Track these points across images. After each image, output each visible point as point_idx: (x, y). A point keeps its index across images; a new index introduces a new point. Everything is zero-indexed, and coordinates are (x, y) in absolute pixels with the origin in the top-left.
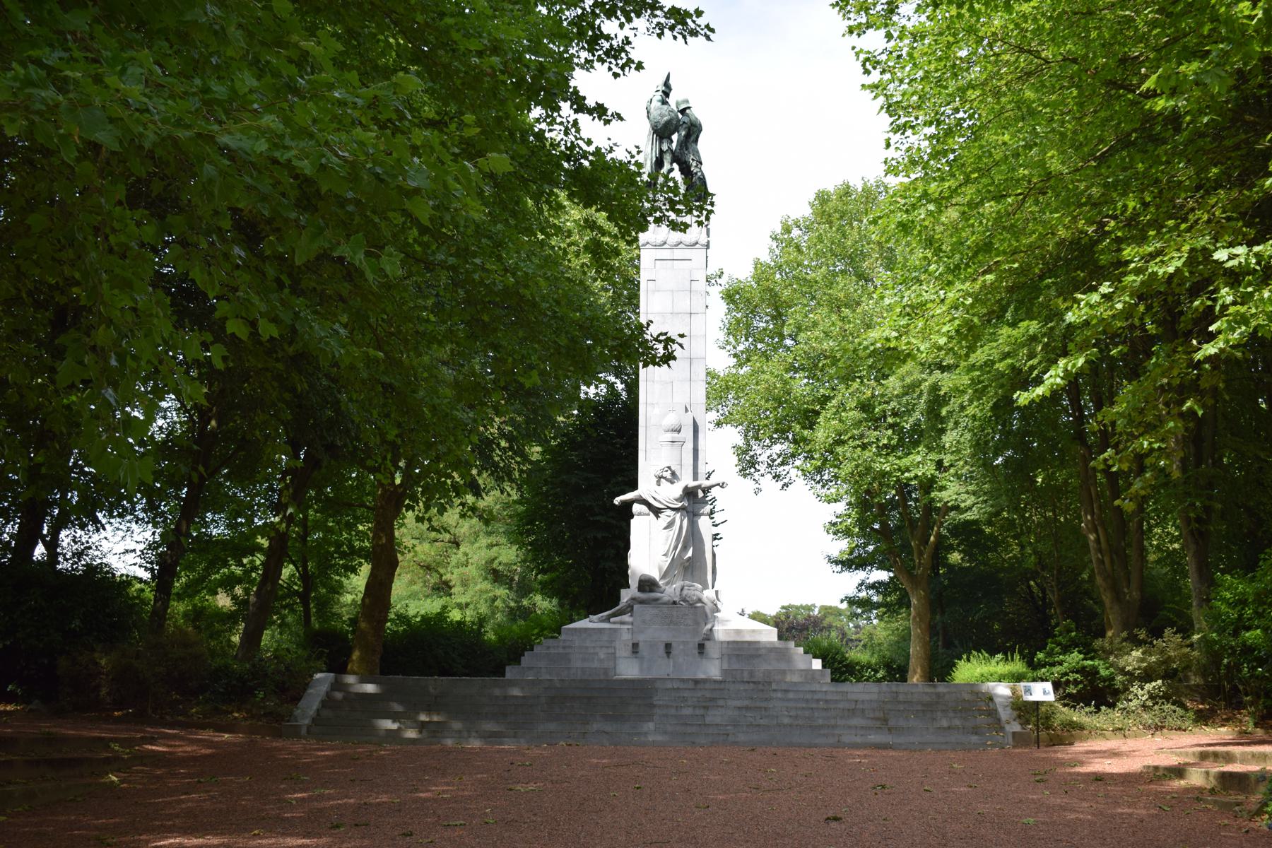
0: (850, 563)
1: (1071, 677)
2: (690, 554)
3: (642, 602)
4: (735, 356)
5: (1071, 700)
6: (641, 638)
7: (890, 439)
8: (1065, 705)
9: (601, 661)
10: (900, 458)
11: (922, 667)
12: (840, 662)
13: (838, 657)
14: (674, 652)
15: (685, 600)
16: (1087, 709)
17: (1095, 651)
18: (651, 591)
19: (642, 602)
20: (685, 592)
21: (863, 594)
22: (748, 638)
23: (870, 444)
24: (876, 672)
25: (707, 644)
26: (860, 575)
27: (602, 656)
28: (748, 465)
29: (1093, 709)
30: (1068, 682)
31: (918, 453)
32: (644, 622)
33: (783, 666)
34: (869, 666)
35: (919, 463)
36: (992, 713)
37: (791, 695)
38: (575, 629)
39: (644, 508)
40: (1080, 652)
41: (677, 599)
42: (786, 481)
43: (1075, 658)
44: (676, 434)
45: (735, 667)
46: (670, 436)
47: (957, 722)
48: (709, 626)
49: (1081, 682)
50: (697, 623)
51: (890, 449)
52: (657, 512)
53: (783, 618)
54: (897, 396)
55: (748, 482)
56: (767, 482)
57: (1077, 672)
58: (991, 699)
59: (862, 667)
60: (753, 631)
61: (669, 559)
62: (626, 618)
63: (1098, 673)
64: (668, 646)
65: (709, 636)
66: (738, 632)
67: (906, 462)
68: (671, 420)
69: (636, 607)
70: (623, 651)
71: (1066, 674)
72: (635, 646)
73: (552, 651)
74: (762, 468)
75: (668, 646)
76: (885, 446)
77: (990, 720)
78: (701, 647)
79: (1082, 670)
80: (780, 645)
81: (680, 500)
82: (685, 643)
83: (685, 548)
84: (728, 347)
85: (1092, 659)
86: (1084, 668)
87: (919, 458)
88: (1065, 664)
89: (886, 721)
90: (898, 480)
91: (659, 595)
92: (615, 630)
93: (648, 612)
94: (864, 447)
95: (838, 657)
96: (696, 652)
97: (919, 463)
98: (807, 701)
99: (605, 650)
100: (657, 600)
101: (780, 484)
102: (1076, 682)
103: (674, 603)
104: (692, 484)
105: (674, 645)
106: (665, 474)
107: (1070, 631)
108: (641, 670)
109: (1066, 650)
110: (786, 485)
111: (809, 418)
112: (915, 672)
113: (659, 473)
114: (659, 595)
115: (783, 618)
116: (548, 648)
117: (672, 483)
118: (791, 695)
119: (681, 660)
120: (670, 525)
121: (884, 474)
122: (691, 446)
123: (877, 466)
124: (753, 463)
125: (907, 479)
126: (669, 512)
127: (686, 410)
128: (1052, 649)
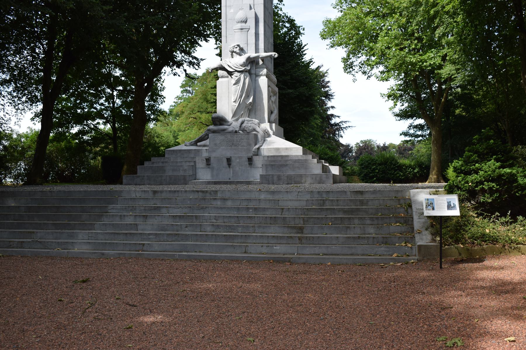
0: (403, 115)
1: (486, 186)
2: (251, 100)
3: (214, 132)
4: (341, 11)
5: (487, 210)
6: (213, 155)
7: (416, 45)
8: (479, 215)
9: (185, 170)
10: (421, 55)
11: (438, 168)
12: (394, 165)
13: (394, 162)
14: (233, 164)
15: (243, 130)
16: (503, 219)
17: (515, 159)
18: (221, 124)
19: (214, 132)
20: (244, 125)
21: (412, 131)
22: (283, 154)
23: (405, 47)
24: (414, 169)
25: (255, 158)
26: (410, 121)
27: (185, 168)
28: (348, 67)
29: (508, 219)
30: (483, 191)
31: (432, 52)
32: (216, 145)
33: (302, 172)
34: (410, 166)
35: (432, 57)
36: (408, 221)
37: (229, 204)
38: (174, 150)
39: (225, 73)
40: (497, 160)
41: (237, 129)
42: (369, 75)
43: (491, 166)
44: (243, 24)
45: (270, 173)
46: (239, 26)
47: (371, 230)
48: (257, 146)
49: (497, 191)
50: (250, 145)
51: (416, 51)
52: (230, 74)
53: (402, 145)
54: (406, 7)
55: (350, 77)
56: (360, 76)
57: (493, 181)
58: (410, 206)
59: (407, 167)
60: (287, 149)
61: (237, 105)
62: (207, 142)
63: (516, 181)
64: (229, 160)
65: (257, 152)
66: (278, 149)
67: (425, 57)
68: (240, 15)
69: (210, 135)
70: (201, 164)
71: (481, 183)
72: (208, 160)
73: (155, 165)
74: (357, 69)
75: (229, 160)
76: (414, 49)
77: (404, 228)
78: (250, 160)
79: (498, 179)
80: (305, 157)
81: (244, 65)
82: (240, 158)
83: (248, 96)
84: (337, 7)
85: (511, 166)
86: (500, 176)
87: (432, 55)
88: (481, 173)
89: (301, 230)
90: (421, 67)
91: (226, 127)
92: (198, 151)
93: (219, 138)
94: (401, 49)
95: (394, 162)
96: (247, 163)
97: (432, 57)
98: (238, 209)
99: (188, 164)
100: (224, 130)
101: (367, 76)
102: (491, 191)
103: (236, 132)
104: (253, 55)
105: (233, 159)
106: (235, 50)
107: (489, 138)
108: (212, 176)
109: (483, 158)
110: (369, 77)
111: (374, 39)
112: (434, 169)
113: (231, 49)
114: (226, 127)
115: (402, 145)
116: (153, 163)
117: (240, 55)
118: (229, 204)
119: (237, 169)
120: (237, 82)
121: (412, 64)
122: (254, 31)
123: (408, 59)
124: (351, 66)
125: (425, 66)
126: (236, 74)
127: (251, 8)
128: (469, 157)
